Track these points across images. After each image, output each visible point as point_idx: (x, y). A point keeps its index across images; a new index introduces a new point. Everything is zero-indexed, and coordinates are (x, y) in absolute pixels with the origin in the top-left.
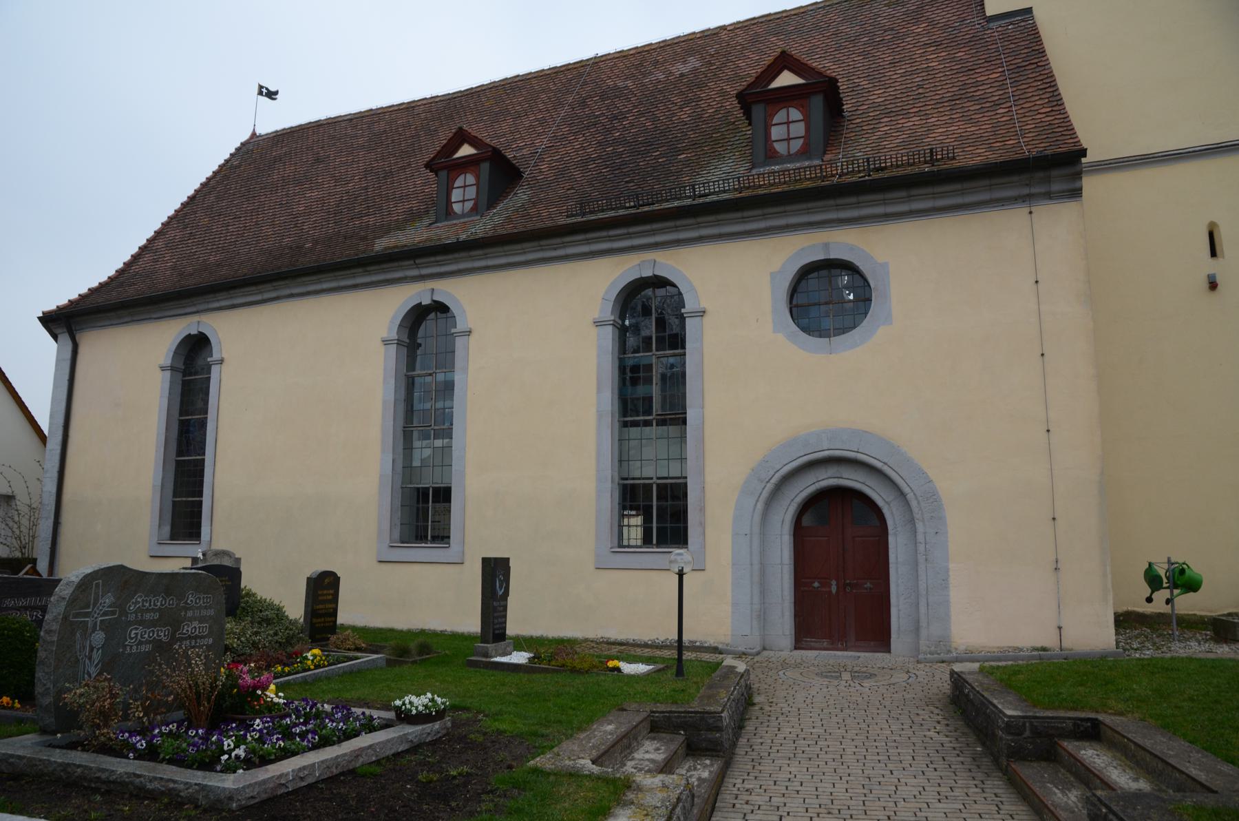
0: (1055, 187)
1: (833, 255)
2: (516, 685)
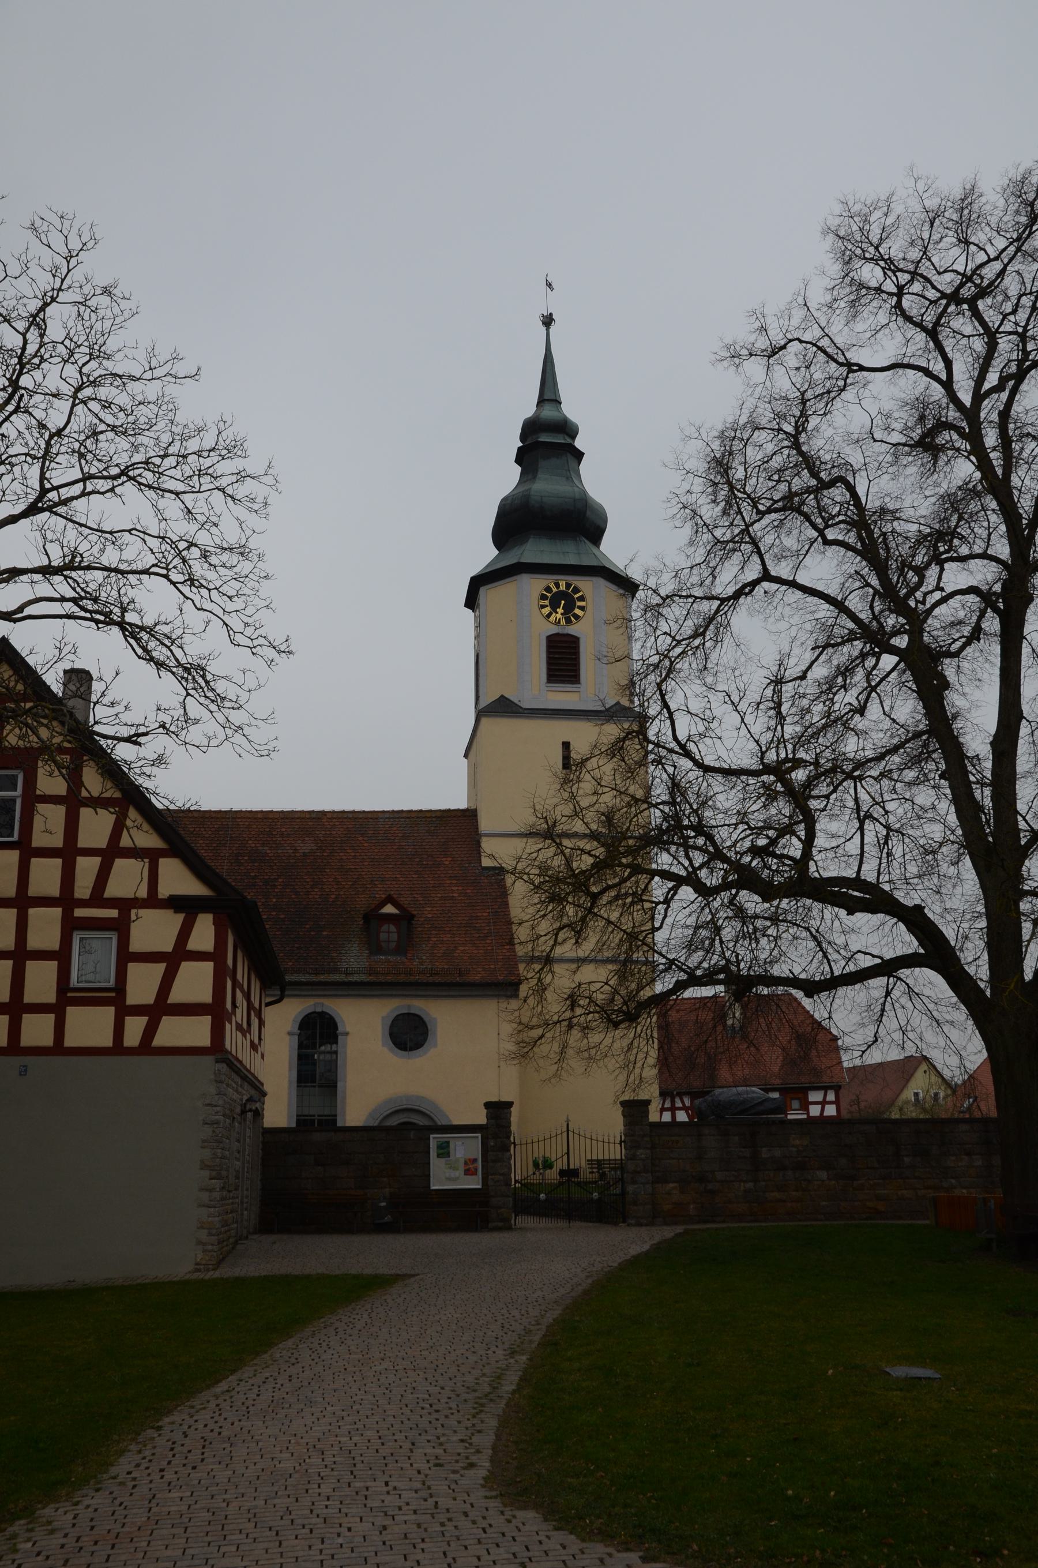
0: (509, 993)
1: (412, 1012)
2: (631, 806)
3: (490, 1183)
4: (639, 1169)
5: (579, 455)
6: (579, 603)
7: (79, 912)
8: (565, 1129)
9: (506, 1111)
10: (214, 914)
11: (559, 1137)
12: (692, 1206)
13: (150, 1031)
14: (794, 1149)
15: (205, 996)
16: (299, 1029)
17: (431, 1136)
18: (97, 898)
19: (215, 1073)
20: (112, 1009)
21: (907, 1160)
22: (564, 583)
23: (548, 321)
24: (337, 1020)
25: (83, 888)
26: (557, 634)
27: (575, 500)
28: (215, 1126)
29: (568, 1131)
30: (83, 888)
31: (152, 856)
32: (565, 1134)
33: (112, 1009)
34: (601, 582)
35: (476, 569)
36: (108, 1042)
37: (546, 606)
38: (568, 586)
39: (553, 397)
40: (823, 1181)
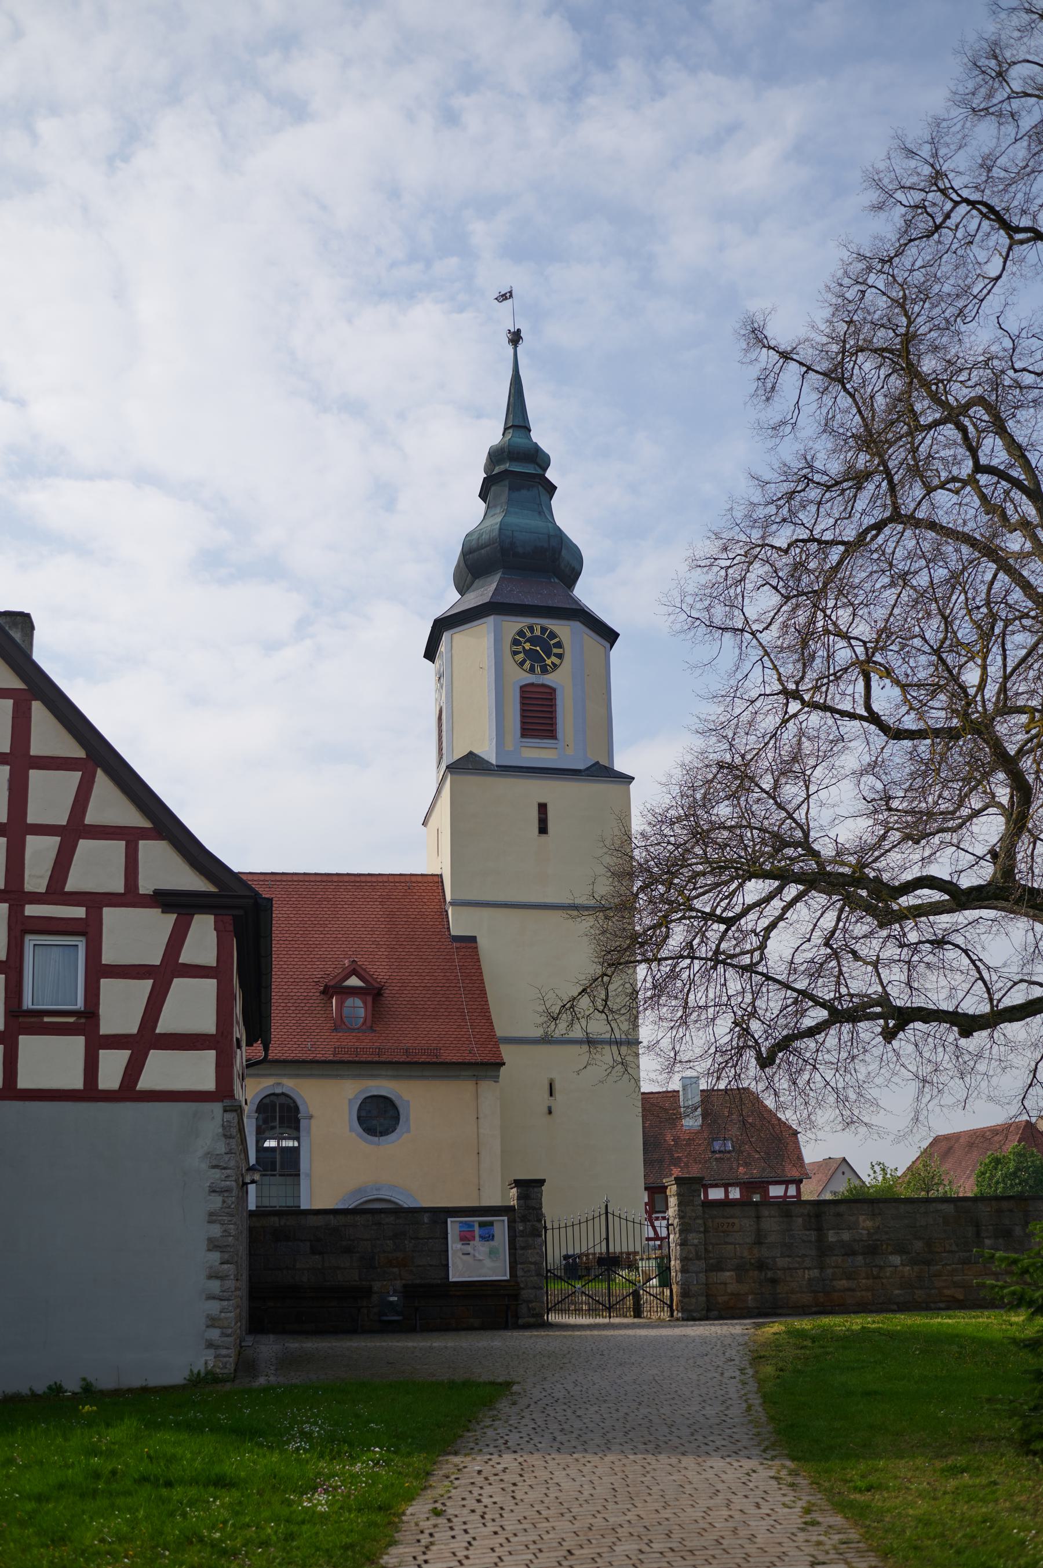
3: (520, 1273)
4: (691, 1256)
5: (551, 489)
6: (555, 651)
7: (31, 910)
8: (603, 1211)
9: (536, 1190)
10: (215, 915)
11: (597, 1220)
12: (750, 1297)
13: (133, 1070)
14: (865, 1232)
15: (208, 1025)
16: (256, 1112)
17: (449, 1220)
18: (56, 892)
19: (223, 1126)
20: (81, 1039)
21: (987, 1242)
22: (539, 627)
23: (515, 338)
24: (299, 1102)
25: (36, 879)
26: (532, 685)
27: (549, 536)
28: (226, 1194)
29: (607, 1213)
30: (36, 879)
31: (130, 836)
32: (603, 1217)
33: (81, 1039)
34: (577, 625)
35: (441, 609)
36: (77, 1082)
37: (520, 652)
38: (544, 630)
39: (522, 424)
40: (896, 1267)
